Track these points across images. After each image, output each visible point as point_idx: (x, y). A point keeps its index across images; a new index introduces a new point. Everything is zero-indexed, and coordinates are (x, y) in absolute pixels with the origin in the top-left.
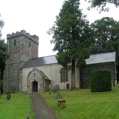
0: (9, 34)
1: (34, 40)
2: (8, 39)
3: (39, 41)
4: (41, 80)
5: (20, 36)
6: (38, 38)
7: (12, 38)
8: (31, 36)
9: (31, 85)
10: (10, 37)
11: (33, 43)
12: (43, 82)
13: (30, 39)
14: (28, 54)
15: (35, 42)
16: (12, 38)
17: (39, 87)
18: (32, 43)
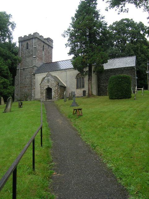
0: (21, 37)
1: (48, 43)
2: (19, 42)
3: (54, 44)
4: (56, 86)
5: (33, 38)
6: (52, 41)
7: (24, 41)
8: (45, 39)
9: (44, 92)
10: (22, 40)
11: (47, 46)
12: (58, 88)
13: (44, 42)
14: (41, 59)
15: (49, 46)
16: (24, 41)
17: (53, 93)
18: (46, 46)
